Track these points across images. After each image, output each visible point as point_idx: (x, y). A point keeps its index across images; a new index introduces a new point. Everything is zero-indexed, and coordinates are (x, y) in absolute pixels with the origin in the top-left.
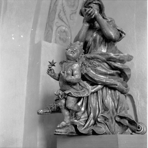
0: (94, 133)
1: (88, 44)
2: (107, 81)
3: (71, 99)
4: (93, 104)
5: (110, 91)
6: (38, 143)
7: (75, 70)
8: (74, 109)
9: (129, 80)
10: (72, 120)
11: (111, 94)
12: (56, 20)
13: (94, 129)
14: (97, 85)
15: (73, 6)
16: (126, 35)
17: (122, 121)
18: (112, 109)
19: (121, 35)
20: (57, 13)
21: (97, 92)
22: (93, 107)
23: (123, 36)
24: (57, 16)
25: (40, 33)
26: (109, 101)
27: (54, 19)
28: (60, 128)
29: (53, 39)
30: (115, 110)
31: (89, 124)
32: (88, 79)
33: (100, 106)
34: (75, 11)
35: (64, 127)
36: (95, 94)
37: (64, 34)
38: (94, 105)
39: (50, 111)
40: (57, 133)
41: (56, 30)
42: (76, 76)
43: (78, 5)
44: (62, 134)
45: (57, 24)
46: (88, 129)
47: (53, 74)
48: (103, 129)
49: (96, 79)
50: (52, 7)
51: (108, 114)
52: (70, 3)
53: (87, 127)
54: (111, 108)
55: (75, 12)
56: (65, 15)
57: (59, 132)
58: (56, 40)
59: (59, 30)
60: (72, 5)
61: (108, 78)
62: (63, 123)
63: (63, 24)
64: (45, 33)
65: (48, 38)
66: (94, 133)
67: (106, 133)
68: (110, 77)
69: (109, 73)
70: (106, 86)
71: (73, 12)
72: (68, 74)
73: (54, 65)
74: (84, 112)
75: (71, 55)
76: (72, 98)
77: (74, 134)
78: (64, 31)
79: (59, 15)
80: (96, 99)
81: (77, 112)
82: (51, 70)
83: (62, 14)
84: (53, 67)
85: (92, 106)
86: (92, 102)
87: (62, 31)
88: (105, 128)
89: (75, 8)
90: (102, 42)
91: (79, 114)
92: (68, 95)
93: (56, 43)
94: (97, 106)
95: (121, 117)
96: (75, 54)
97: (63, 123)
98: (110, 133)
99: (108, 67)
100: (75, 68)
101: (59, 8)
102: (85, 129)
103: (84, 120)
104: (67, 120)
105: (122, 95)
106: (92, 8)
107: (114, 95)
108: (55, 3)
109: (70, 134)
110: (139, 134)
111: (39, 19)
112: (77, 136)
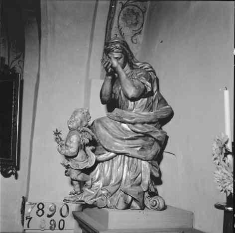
4: (105, 172)
15: (136, 24)
36: (111, 160)
52: (130, 21)
60: (134, 23)
71: (137, 32)
73: (59, 133)
86: (106, 169)
89: (139, 26)
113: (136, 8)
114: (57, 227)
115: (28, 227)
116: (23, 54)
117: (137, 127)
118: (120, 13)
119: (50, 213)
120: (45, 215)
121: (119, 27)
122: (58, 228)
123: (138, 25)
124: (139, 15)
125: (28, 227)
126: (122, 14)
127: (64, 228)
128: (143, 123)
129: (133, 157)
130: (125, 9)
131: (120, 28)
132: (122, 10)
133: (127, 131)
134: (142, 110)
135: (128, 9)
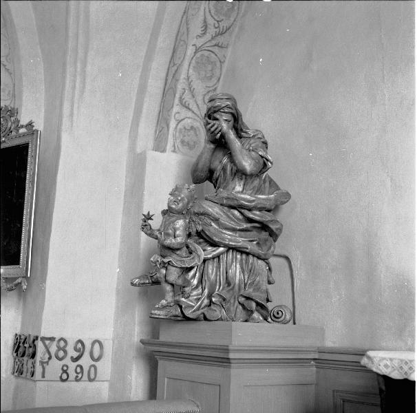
0: (206, 319)
1: (215, 175)
2: (231, 243)
3: (172, 269)
4: (210, 276)
5: (239, 256)
6: (136, 330)
7: (178, 229)
8: (178, 283)
9: (279, 239)
10: (177, 298)
11: (241, 260)
12: (176, 109)
13: (206, 313)
14: (219, 246)
15: (211, 78)
16: (274, 165)
17: (246, 303)
18: (239, 284)
19: (265, 165)
20: (178, 96)
21: (219, 257)
22: (209, 281)
23: (268, 167)
24: (177, 101)
25: (147, 130)
26: (236, 272)
27: (172, 107)
28: (158, 309)
29: (169, 147)
30: (243, 286)
31: (200, 305)
32: (205, 237)
33: (222, 279)
34: (212, 87)
35: (164, 307)
36: (216, 260)
37: (192, 132)
38: (213, 277)
39: (150, 281)
40: (153, 316)
41: (176, 128)
42: (178, 238)
43: (221, 75)
44: (161, 317)
45: (177, 116)
46: (199, 312)
47: (149, 232)
48: (218, 312)
49: (214, 238)
50: (169, 81)
51: (228, 291)
52: (204, 73)
53: (198, 309)
54: (237, 281)
55: (213, 88)
56: (193, 96)
57: (156, 314)
58: (174, 146)
59: (179, 126)
60: (208, 75)
61: (237, 235)
62: (164, 302)
63: (190, 114)
64: (156, 132)
65: (160, 146)
66: (206, 319)
67: (221, 319)
68: (242, 233)
69: (238, 228)
70: (230, 248)
71: (211, 89)
72: (168, 235)
73: (150, 219)
74: (197, 287)
75: (174, 206)
76: (174, 268)
77: (179, 318)
78: (192, 128)
79: (181, 99)
80: (217, 267)
81: (184, 287)
82: (146, 225)
83: (187, 97)
84: (150, 221)
85: (209, 278)
86: (210, 271)
87: (186, 128)
88: (220, 311)
89: (214, 80)
90: (235, 174)
91: (186, 289)
92: (169, 263)
93: (174, 151)
94: (218, 278)
95: (248, 298)
96: (181, 205)
97: (164, 302)
98: (229, 319)
99: (241, 217)
100: (178, 226)
101: (181, 86)
102: (194, 311)
103: (196, 299)
104: (169, 297)
105: (260, 261)
106: (217, 119)
107: (246, 263)
108: (174, 74)
109: (172, 318)
110: (279, 322)
111: (145, 106)
112: (180, 323)
113: (213, 55)
114: (85, 377)
115: (43, 377)
116: (198, 113)
117: (254, 214)
118: (192, 58)
119: (76, 354)
120: (68, 358)
121: (188, 79)
122: (87, 379)
123: (213, 79)
124: (216, 65)
125: (43, 377)
126: (193, 61)
127: (96, 379)
128: (260, 209)
129: (248, 254)
130: (198, 55)
131: (190, 80)
132: (194, 55)
133: (238, 219)
134: (255, 192)
135: (202, 55)
